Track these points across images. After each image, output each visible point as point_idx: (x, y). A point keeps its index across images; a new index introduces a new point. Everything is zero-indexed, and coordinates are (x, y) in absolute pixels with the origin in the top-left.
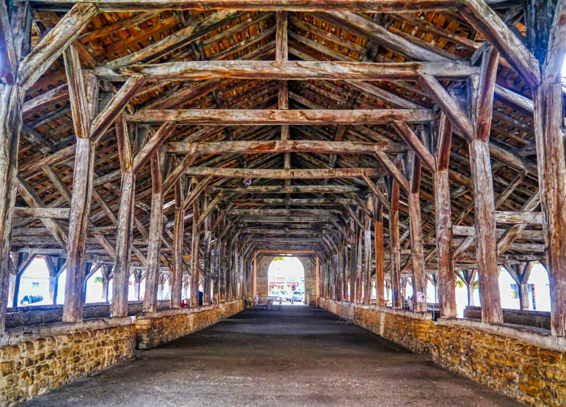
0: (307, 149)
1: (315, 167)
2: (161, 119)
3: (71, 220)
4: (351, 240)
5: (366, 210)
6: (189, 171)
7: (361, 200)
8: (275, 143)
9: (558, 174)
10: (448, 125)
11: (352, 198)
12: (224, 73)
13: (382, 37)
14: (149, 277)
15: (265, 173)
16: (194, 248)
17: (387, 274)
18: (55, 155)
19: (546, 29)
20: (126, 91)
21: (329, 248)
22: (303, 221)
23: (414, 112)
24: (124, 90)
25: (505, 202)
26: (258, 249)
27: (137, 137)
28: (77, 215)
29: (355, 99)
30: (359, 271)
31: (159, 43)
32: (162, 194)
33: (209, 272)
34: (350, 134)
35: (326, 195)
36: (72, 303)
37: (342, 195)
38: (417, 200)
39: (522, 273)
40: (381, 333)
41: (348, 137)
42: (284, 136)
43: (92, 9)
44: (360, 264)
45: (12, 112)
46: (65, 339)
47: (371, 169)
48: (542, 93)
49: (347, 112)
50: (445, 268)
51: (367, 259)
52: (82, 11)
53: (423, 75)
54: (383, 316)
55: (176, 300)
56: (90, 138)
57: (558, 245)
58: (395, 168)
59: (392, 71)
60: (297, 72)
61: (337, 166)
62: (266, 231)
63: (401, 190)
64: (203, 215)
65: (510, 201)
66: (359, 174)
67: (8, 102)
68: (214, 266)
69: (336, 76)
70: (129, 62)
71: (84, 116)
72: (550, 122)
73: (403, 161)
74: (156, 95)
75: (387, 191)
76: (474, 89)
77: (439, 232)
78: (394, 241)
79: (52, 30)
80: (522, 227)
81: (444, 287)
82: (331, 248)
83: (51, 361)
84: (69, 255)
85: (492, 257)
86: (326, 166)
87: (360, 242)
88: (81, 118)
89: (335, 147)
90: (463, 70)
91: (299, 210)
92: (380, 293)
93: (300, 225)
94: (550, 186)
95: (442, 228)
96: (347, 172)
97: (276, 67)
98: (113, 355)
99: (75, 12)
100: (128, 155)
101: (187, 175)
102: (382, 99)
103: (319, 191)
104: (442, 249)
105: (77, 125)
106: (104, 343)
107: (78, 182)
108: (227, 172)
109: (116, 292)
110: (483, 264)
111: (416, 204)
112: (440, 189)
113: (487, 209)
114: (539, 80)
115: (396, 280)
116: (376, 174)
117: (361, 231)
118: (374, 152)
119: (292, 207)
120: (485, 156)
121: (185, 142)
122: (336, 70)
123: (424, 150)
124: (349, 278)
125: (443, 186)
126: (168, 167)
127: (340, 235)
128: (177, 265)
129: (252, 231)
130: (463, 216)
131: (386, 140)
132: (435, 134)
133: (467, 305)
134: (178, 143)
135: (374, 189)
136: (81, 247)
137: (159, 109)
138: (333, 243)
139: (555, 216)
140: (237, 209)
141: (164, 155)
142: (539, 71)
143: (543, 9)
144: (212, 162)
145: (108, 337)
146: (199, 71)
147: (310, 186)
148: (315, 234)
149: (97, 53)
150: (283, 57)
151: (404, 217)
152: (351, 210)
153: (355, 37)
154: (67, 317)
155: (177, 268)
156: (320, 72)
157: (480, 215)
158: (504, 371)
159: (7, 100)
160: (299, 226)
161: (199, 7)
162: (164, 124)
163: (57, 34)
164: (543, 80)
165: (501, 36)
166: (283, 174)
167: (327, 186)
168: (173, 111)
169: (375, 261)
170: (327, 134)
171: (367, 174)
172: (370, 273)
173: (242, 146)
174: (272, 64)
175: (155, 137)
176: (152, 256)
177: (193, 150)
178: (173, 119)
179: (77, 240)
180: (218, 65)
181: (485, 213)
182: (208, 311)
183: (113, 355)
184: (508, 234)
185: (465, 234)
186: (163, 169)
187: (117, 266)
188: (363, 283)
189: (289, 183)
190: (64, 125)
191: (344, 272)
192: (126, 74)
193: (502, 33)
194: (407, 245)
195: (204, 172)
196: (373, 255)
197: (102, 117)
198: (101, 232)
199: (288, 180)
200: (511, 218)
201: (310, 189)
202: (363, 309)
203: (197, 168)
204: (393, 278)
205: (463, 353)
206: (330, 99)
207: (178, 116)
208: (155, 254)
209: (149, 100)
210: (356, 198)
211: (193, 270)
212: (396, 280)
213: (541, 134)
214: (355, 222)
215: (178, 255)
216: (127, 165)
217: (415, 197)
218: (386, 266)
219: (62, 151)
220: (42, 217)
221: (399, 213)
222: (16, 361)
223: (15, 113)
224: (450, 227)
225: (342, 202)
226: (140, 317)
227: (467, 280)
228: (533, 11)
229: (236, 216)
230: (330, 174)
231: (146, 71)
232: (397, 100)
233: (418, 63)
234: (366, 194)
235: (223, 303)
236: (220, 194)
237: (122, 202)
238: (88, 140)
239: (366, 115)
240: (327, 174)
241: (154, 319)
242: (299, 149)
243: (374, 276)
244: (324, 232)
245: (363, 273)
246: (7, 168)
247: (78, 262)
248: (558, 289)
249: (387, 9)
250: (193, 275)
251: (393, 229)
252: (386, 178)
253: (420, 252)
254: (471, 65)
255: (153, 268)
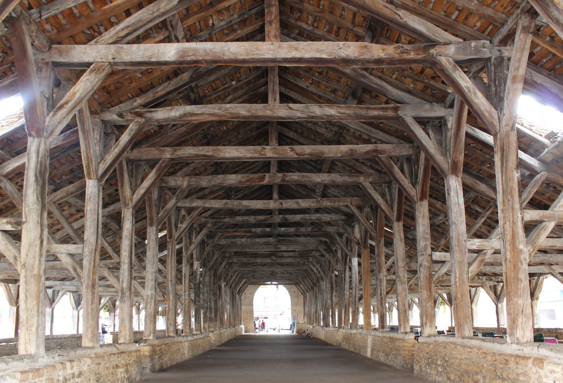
0: (296, 181)
1: (302, 197)
2: (158, 157)
3: (84, 255)
4: (339, 266)
5: (353, 237)
6: (179, 205)
7: (347, 227)
8: (265, 175)
9: (513, 209)
10: (427, 160)
11: (338, 226)
12: (220, 116)
13: (365, 81)
14: (148, 307)
15: (254, 203)
16: (185, 278)
17: (374, 299)
18: (59, 192)
19: (503, 84)
20: (130, 134)
21: (316, 275)
22: (290, 249)
23: (397, 146)
24: (128, 134)
25: (480, 227)
26: (244, 278)
27: (134, 173)
28: (90, 251)
29: (341, 133)
30: (347, 297)
31: (160, 89)
32: (157, 227)
33: (199, 302)
34: (337, 165)
35: (312, 224)
36: (90, 331)
37: (329, 223)
38: (401, 228)
39: (499, 293)
40: (369, 355)
41: (335, 168)
42: (273, 169)
43: (107, 68)
44: (348, 290)
45: (41, 162)
46: (89, 361)
47: (358, 198)
48: (501, 140)
49: (334, 148)
50: (425, 291)
51: (354, 285)
52: (99, 70)
53: (404, 117)
54: (370, 339)
55: (172, 329)
56: (98, 180)
57: (512, 268)
58: (380, 198)
59: (376, 113)
60: (288, 114)
61: (324, 195)
62: (253, 260)
63: (385, 217)
64: (193, 246)
65: (485, 227)
66: (346, 203)
67: (38, 153)
68: (203, 296)
69: (325, 117)
70: (132, 107)
71: (93, 159)
72: (506, 165)
73: (387, 190)
74: (152, 133)
75: (372, 219)
76: (448, 129)
77: (420, 259)
78: (380, 267)
79: (73, 88)
80: (490, 252)
81: (424, 309)
82: (318, 275)
83: (80, 379)
84: (84, 287)
85: (465, 280)
86: (313, 195)
87: (347, 269)
88: (90, 161)
89: (323, 179)
90: (438, 111)
91: (286, 238)
92: (367, 318)
93: (287, 253)
94: (506, 219)
95: (423, 255)
96: (335, 202)
97: (269, 110)
98: (125, 377)
99: (93, 71)
100: (128, 192)
101: (177, 208)
102: (367, 134)
103: (306, 220)
104: (423, 274)
105: (86, 167)
106: (117, 366)
107: (89, 220)
108: (217, 204)
109: (122, 321)
110: (456, 286)
111: (400, 233)
112: (421, 218)
113: (460, 237)
114: (498, 129)
115: (382, 304)
116: (361, 203)
117: (348, 258)
118: (360, 183)
119: (279, 235)
120: (459, 190)
121: (177, 177)
122: (324, 113)
123: (406, 182)
124: (336, 304)
125: (423, 216)
126: (161, 201)
127: (327, 262)
128: (171, 296)
129: (238, 261)
130: (443, 242)
131: (371, 171)
132: (416, 167)
133: (450, 326)
134: (171, 177)
135: (360, 218)
136: (95, 280)
137: (155, 147)
138: (320, 269)
139: (510, 244)
140: (224, 238)
141: (157, 190)
142: (498, 120)
143: (501, 67)
144: (201, 194)
145: (120, 361)
146: (197, 115)
147: (298, 216)
148: (302, 262)
149: (102, 99)
150: (275, 100)
151: (389, 243)
152: (338, 238)
153: (341, 78)
154: (86, 342)
155: (171, 298)
156: (310, 114)
157: (454, 243)
158: (471, 376)
159: (36, 151)
160: (286, 254)
161: (203, 64)
162: (161, 162)
163: (78, 91)
164: (501, 129)
165: (467, 90)
166: (272, 204)
167: (314, 215)
168: (168, 149)
169: (362, 287)
170: (314, 165)
171: (354, 204)
172: (357, 299)
173: (232, 179)
174: (264, 107)
175: (152, 176)
176: (150, 287)
177: (185, 184)
178: (169, 156)
179: (91, 273)
180: (215, 108)
181: (458, 241)
182: (200, 339)
183: (125, 377)
184: (478, 259)
185: (443, 260)
186: (157, 202)
187: (121, 297)
188: (351, 310)
189: (277, 213)
190: (67, 164)
191: (332, 298)
192: (130, 118)
193: (467, 88)
194: (392, 271)
195: (194, 205)
196: (360, 281)
197: (110, 158)
198: (106, 265)
199: (276, 210)
200: (481, 245)
201: (297, 218)
202: (351, 334)
203: (187, 200)
204: (379, 303)
205: (440, 365)
206: (317, 132)
207: (173, 154)
208: (152, 285)
209: (145, 138)
210: (343, 226)
211: (185, 300)
212: (382, 304)
213: (500, 175)
214: (342, 249)
215: (172, 285)
216: (127, 202)
217: (398, 226)
218: (372, 291)
219: (65, 189)
220: (58, 253)
221: (385, 240)
222: (56, 379)
223: (44, 162)
224: (430, 253)
225: (329, 230)
226: (142, 344)
227: (450, 302)
228: (493, 68)
229: (223, 246)
230: (318, 204)
231: (148, 115)
232: (381, 135)
233: (399, 105)
234: (353, 222)
235: (212, 332)
236: (209, 225)
237: (124, 236)
238: (96, 181)
239: (352, 150)
240: (315, 204)
241: (153, 346)
242: (288, 181)
243: (361, 302)
244: (311, 259)
245: (351, 299)
246: (40, 211)
247: (93, 293)
248: (512, 304)
249: (370, 64)
250: (185, 305)
251: (379, 256)
252: (371, 207)
253: (404, 277)
254: (445, 107)
255: (151, 299)
